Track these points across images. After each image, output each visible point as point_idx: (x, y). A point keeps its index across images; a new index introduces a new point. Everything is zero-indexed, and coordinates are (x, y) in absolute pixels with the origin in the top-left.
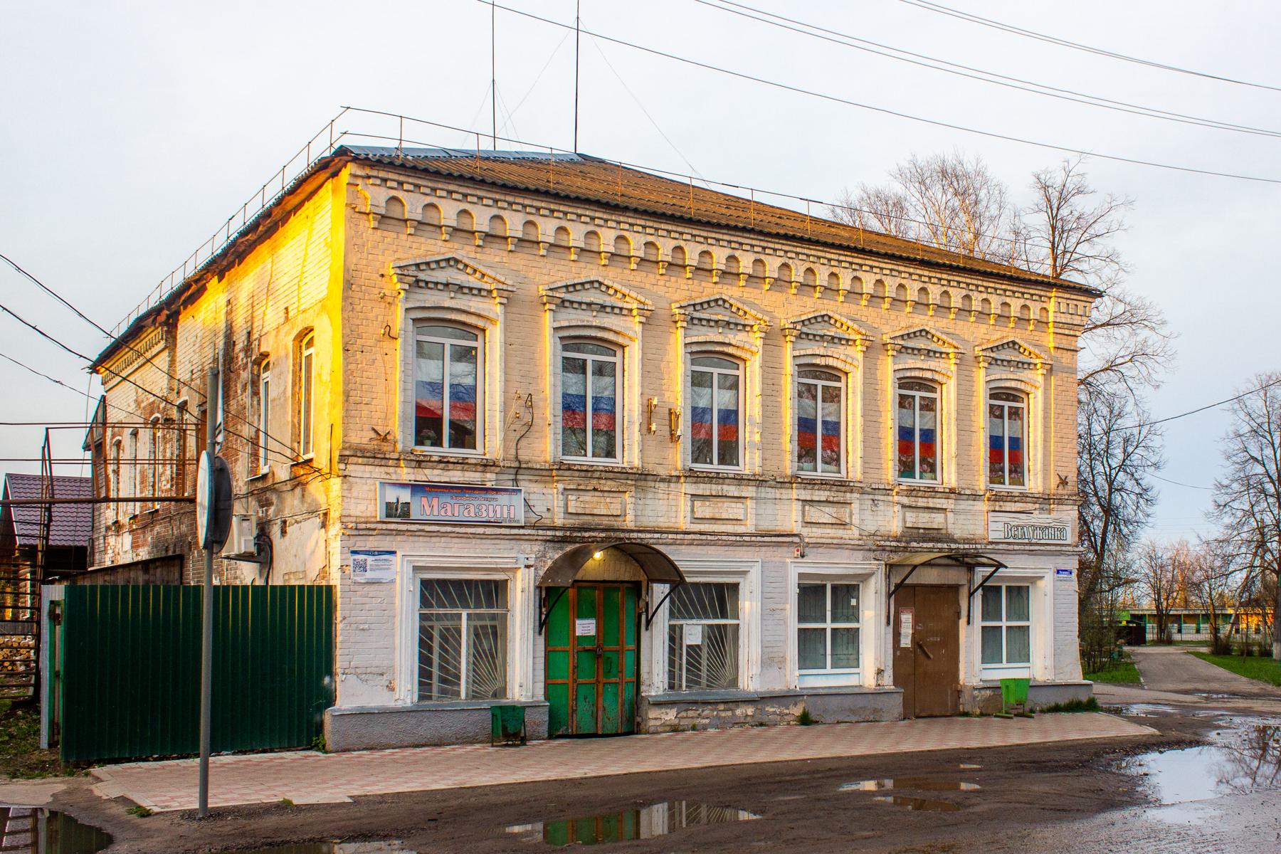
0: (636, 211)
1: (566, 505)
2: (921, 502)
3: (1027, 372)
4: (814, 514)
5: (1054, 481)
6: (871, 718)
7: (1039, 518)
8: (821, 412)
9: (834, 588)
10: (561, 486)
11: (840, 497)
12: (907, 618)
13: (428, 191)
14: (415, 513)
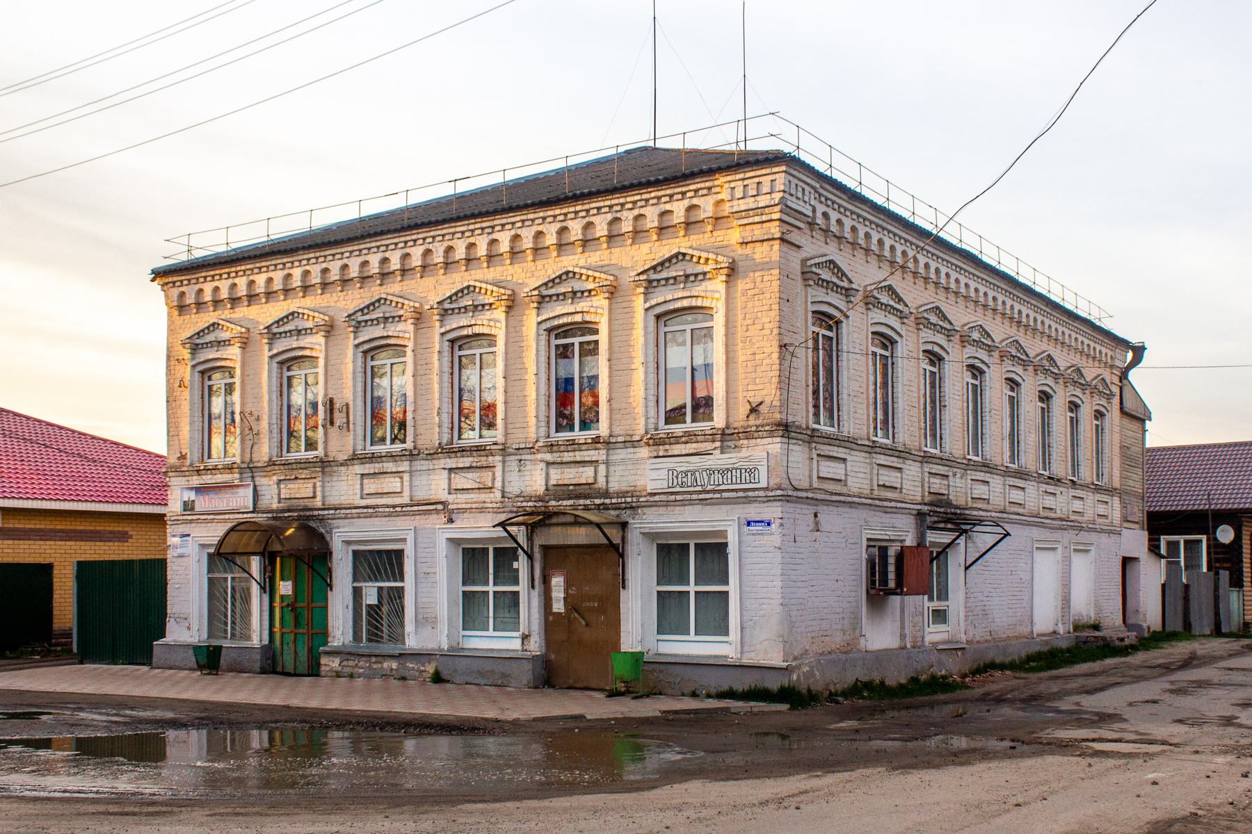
0: (304, 248)
1: (279, 494)
2: (567, 457)
3: (704, 284)
4: (461, 481)
5: (744, 409)
6: (500, 682)
7: (718, 460)
8: (574, 367)
9: (497, 551)
10: (275, 478)
11: (483, 461)
12: (557, 582)
13: (705, 192)
14: (197, 508)
